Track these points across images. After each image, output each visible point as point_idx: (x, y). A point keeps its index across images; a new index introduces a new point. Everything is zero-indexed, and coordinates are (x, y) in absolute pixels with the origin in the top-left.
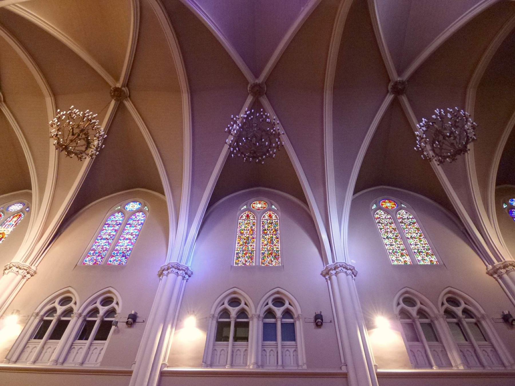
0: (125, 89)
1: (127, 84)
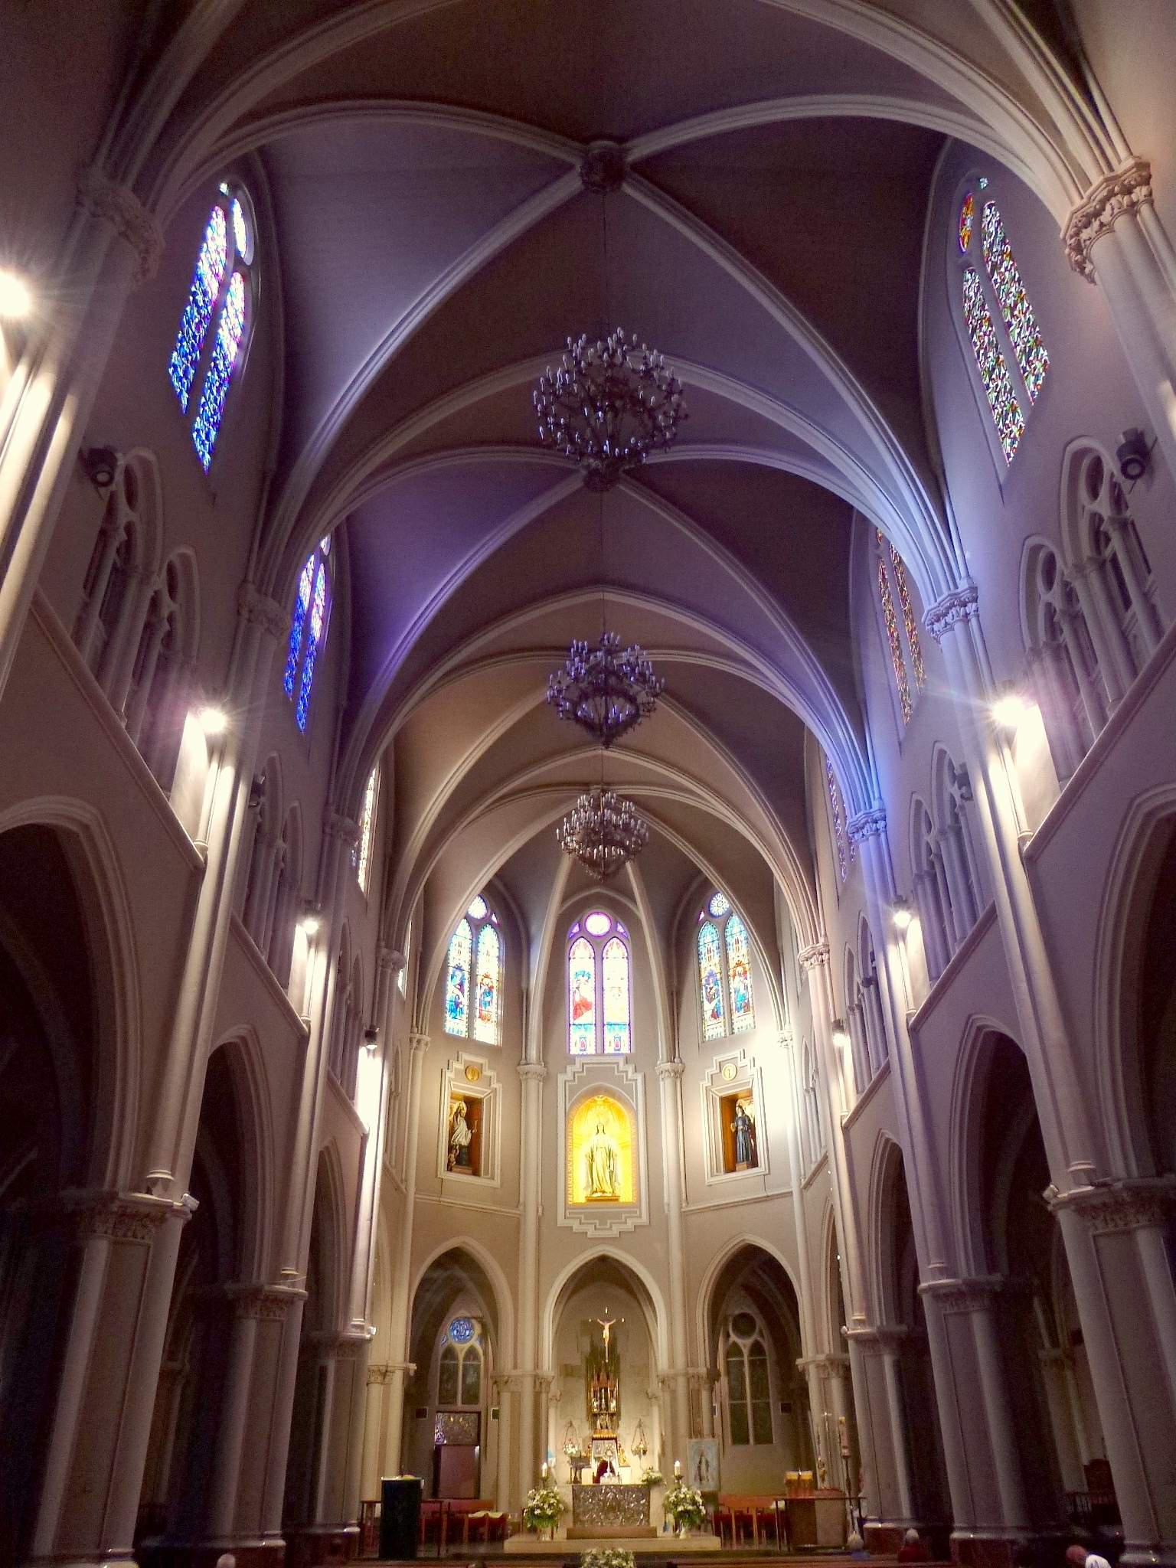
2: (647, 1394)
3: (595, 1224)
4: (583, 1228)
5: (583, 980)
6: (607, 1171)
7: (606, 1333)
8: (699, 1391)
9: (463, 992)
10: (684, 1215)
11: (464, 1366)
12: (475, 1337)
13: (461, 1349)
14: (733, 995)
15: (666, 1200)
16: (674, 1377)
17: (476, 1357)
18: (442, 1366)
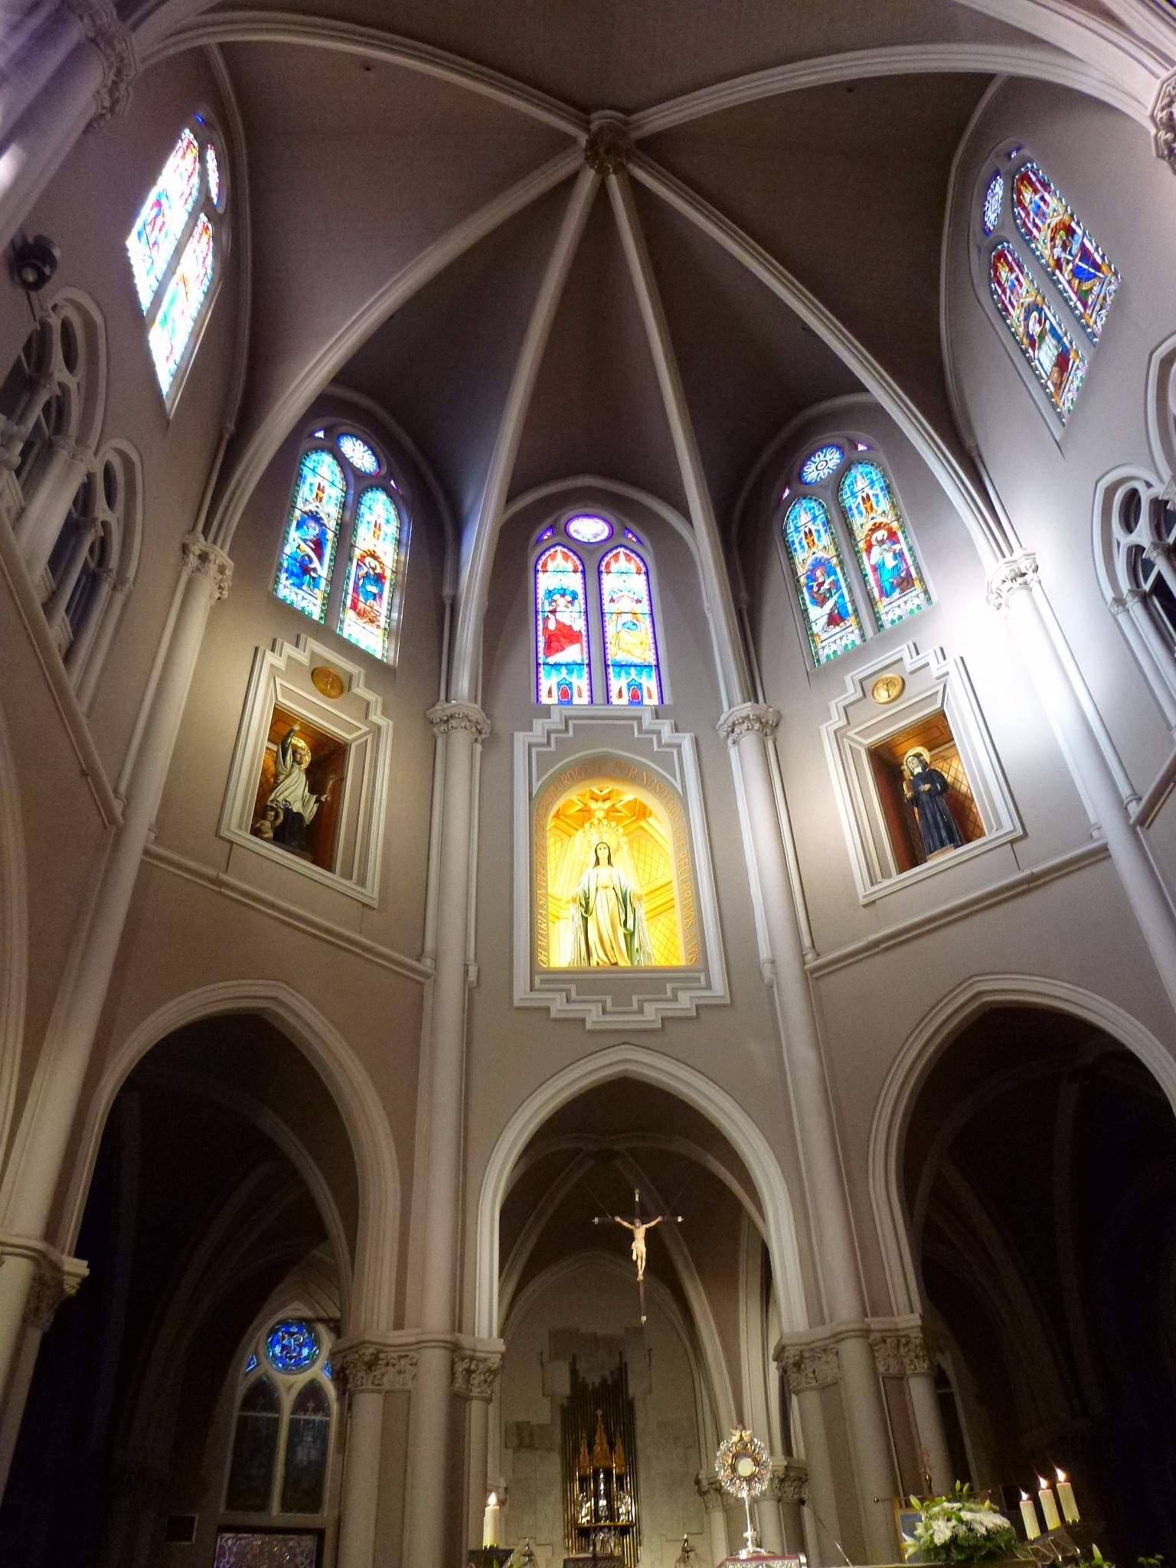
0: (598, 119)
1: (582, 110)
2: (698, 1482)
3: (604, 1003)
4: (575, 1010)
5: (562, 602)
6: (621, 931)
7: (639, 1248)
8: (901, 1378)
9: (320, 557)
10: (813, 977)
11: (294, 1425)
12: (322, 1361)
13: (289, 1385)
14: (871, 578)
15: (764, 953)
16: (830, 1347)
17: (321, 1406)
18: (243, 1422)
